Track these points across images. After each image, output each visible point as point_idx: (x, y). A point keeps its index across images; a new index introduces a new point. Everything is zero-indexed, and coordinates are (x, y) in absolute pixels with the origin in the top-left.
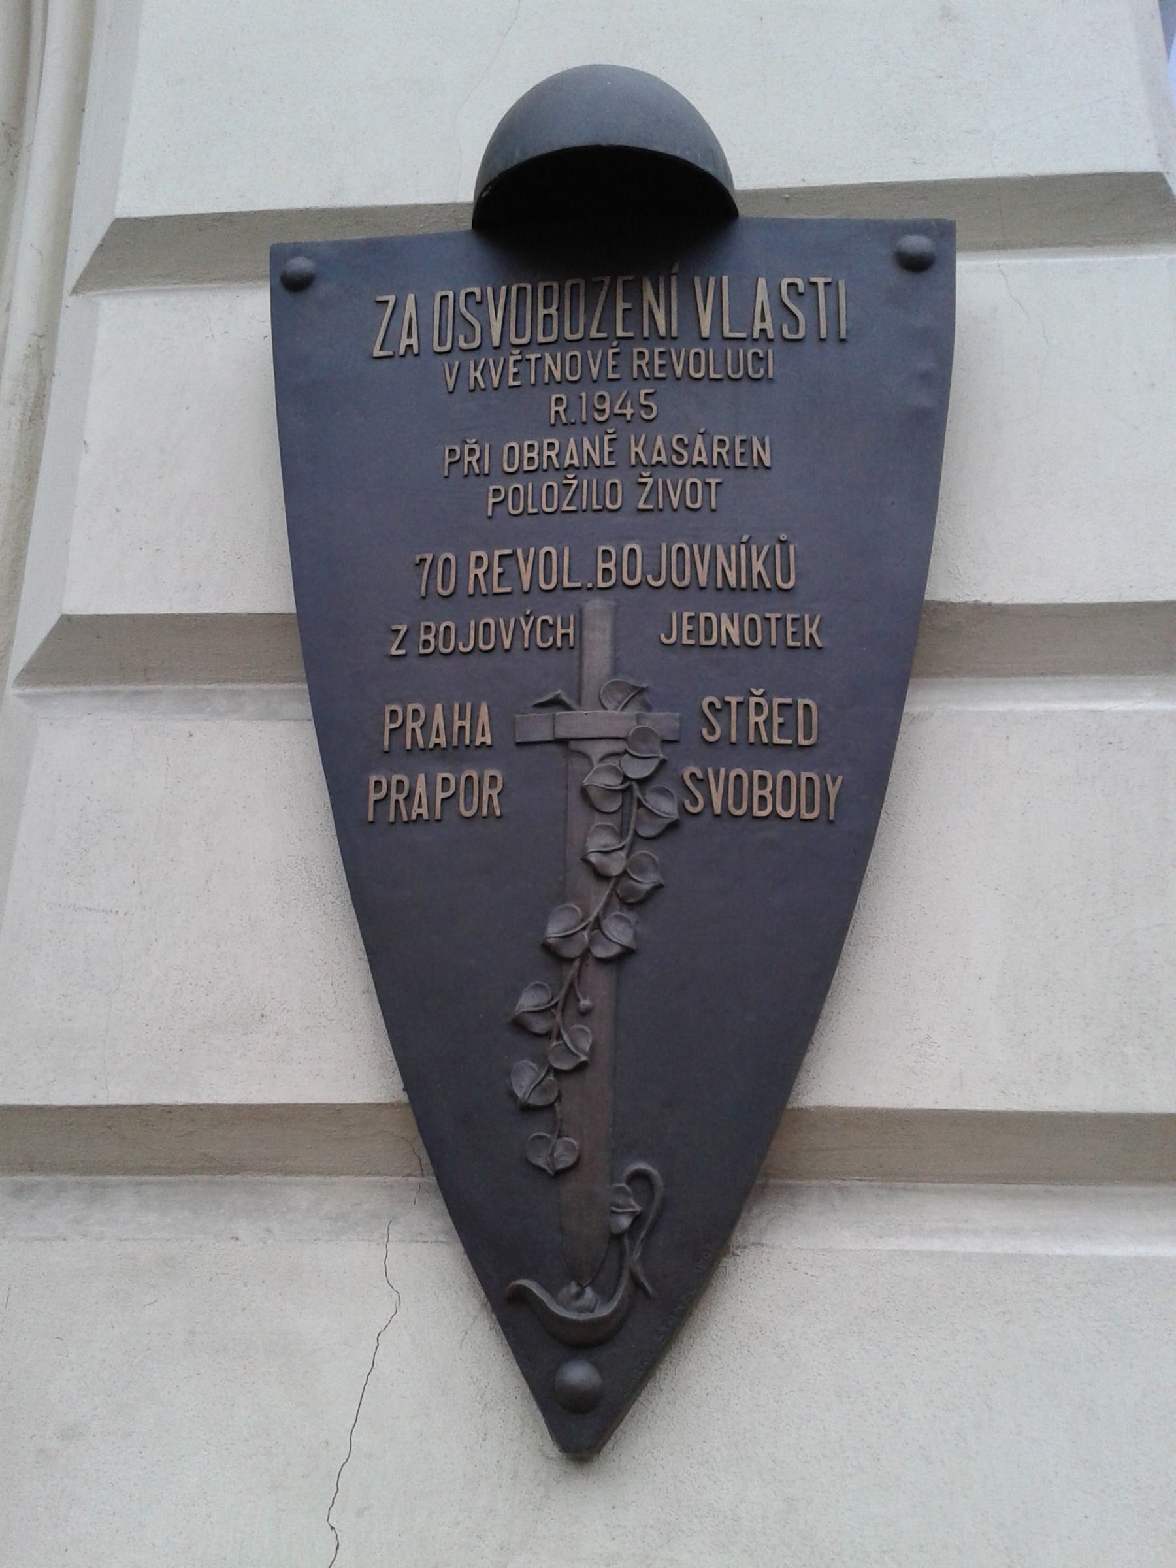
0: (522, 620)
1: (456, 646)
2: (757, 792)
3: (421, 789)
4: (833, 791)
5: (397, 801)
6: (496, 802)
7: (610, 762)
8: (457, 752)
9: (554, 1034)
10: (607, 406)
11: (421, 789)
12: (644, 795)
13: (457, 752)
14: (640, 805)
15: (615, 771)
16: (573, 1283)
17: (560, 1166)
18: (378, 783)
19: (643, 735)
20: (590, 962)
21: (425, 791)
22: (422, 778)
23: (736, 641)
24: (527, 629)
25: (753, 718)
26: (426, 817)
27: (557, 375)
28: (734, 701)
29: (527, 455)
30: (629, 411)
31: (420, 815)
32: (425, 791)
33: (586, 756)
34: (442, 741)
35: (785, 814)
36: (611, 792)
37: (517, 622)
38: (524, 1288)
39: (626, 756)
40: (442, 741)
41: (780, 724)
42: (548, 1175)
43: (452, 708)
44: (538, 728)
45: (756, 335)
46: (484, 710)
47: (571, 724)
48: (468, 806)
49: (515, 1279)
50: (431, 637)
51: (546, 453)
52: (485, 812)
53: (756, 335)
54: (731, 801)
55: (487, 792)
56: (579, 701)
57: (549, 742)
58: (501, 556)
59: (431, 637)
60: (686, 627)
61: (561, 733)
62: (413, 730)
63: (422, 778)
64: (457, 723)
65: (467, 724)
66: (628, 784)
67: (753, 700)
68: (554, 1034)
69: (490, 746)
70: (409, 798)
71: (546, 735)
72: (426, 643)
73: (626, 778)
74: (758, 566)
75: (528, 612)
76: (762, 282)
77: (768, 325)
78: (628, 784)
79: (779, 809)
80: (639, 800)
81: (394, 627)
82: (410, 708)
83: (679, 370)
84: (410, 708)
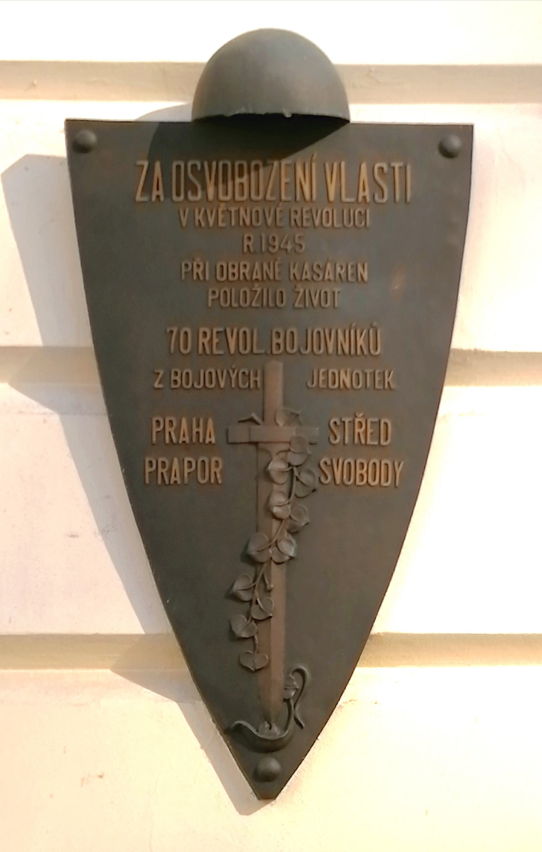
0: (231, 372)
1: (193, 385)
2: (359, 472)
3: (176, 466)
4: (398, 471)
5: (162, 474)
6: (218, 476)
7: (282, 455)
8: (195, 446)
9: (254, 601)
10: (276, 243)
11: (176, 466)
12: (299, 474)
13: (195, 446)
14: (297, 479)
15: (283, 460)
16: (266, 723)
17: (258, 668)
18: (151, 462)
19: (299, 440)
20: (273, 564)
21: (178, 468)
22: (176, 460)
23: (348, 385)
24: (234, 376)
25: (357, 430)
26: (179, 482)
27: (248, 222)
28: (347, 420)
29: (231, 270)
30: (289, 247)
31: (176, 482)
32: (178, 468)
33: (268, 452)
34: (187, 439)
35: (373, 484)
36: (283, 472)
37: (228, 372)
38: (240, 724)
39: (290, 453)
40: (187, 439)
41: (286, 183)
42: (252, 671)
43: (192, 421)
44: (240, 433)
45: (360, 199)
46: (210, 422)
47: (259, 433)
48: (204, 477)
49: (236, 720)
50: (178, 378)
51: (242, 271)
52: (213, 480)
53: (360, 199)
54: (345, 477)
55: (213, 469)
56: (263, 419)
57: (245, 443)
58: (218, 332)
59: (178, 378)
60: (322, 378)
61: (255, 439)
62: (162, 474)
63: (176, 460)
64: (195, 430)
65: (201, 431)
66: (291, 468)
67: (357, 420)
68: (254, 601)
69: (214, 444)
70: (170, 471)
71: (245, 439)
72: (175, 382)
73: (290, 465)
74: (360, 342)
75: (234, 367)
76: (364, 166)
77: (367, 193)
78: (291, 468)
79: (370, 481)
80: (297, 477)
81: (156, 371)
82: (167, 419)
83: (317, 222)
84: (167, 419)
